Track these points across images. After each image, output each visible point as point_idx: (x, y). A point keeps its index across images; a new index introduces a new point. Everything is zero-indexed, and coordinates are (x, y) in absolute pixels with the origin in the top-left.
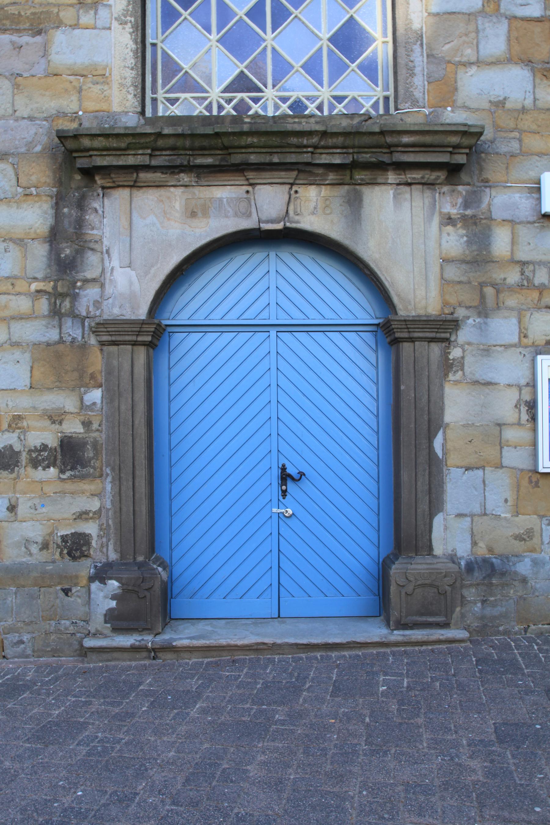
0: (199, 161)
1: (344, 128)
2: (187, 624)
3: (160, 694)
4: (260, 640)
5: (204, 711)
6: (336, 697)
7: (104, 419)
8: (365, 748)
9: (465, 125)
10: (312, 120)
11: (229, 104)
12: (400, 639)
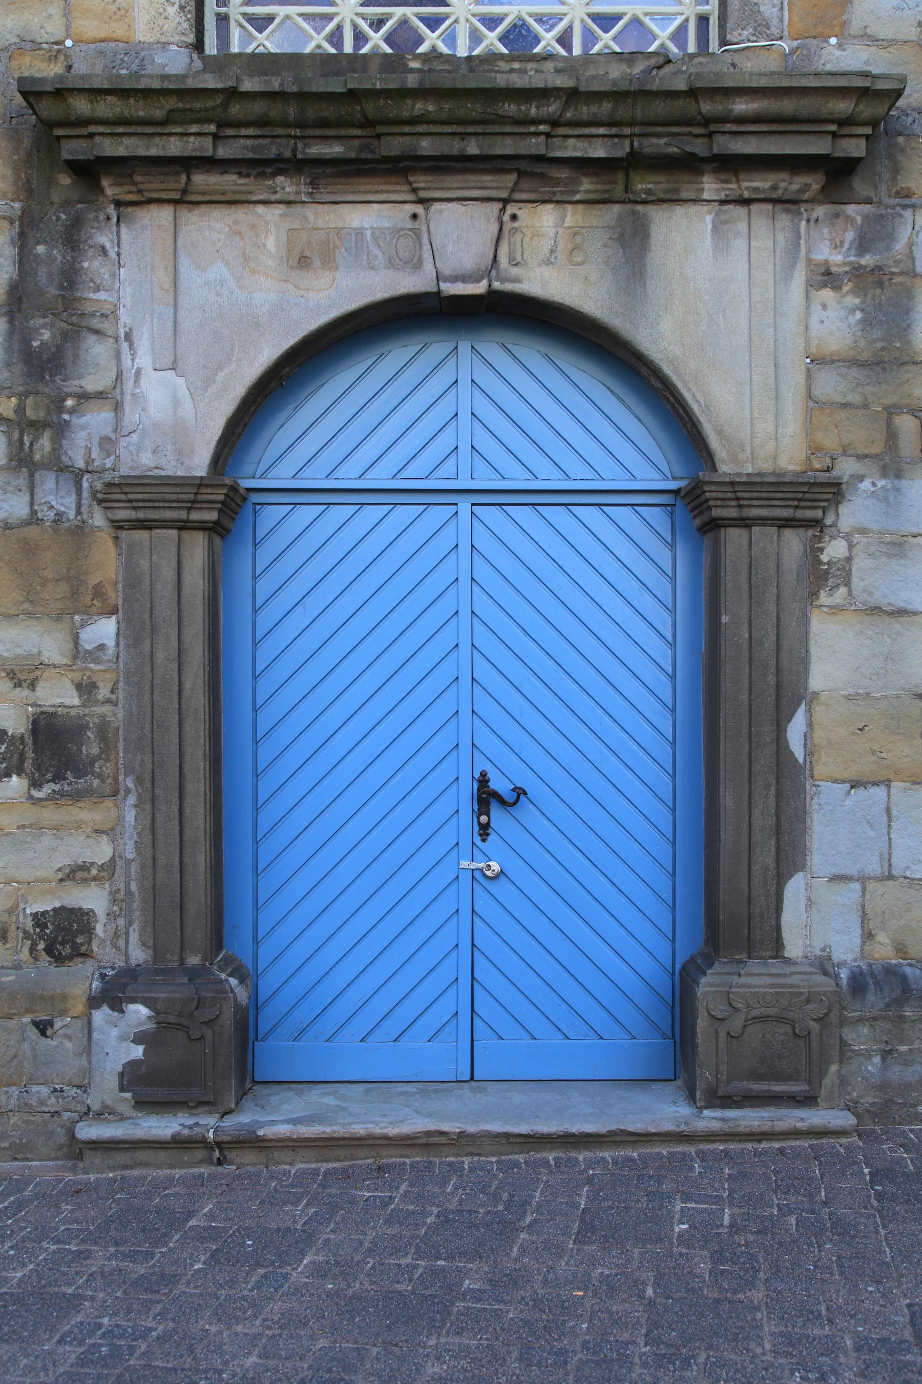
0: (316, 150)
1: (614, 83)
2: (286, 1093)
3: (231, 1236)
4: (432, 1126)
5: (318, 1271)
6: (585, 1243)
7: (121, 679)
8: (644, 1350)
9: (866, 75)
10: (549, 66)
11: (376, 31)
12: (716, 1126)
